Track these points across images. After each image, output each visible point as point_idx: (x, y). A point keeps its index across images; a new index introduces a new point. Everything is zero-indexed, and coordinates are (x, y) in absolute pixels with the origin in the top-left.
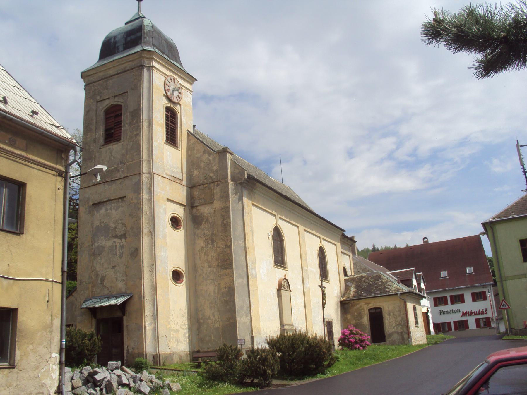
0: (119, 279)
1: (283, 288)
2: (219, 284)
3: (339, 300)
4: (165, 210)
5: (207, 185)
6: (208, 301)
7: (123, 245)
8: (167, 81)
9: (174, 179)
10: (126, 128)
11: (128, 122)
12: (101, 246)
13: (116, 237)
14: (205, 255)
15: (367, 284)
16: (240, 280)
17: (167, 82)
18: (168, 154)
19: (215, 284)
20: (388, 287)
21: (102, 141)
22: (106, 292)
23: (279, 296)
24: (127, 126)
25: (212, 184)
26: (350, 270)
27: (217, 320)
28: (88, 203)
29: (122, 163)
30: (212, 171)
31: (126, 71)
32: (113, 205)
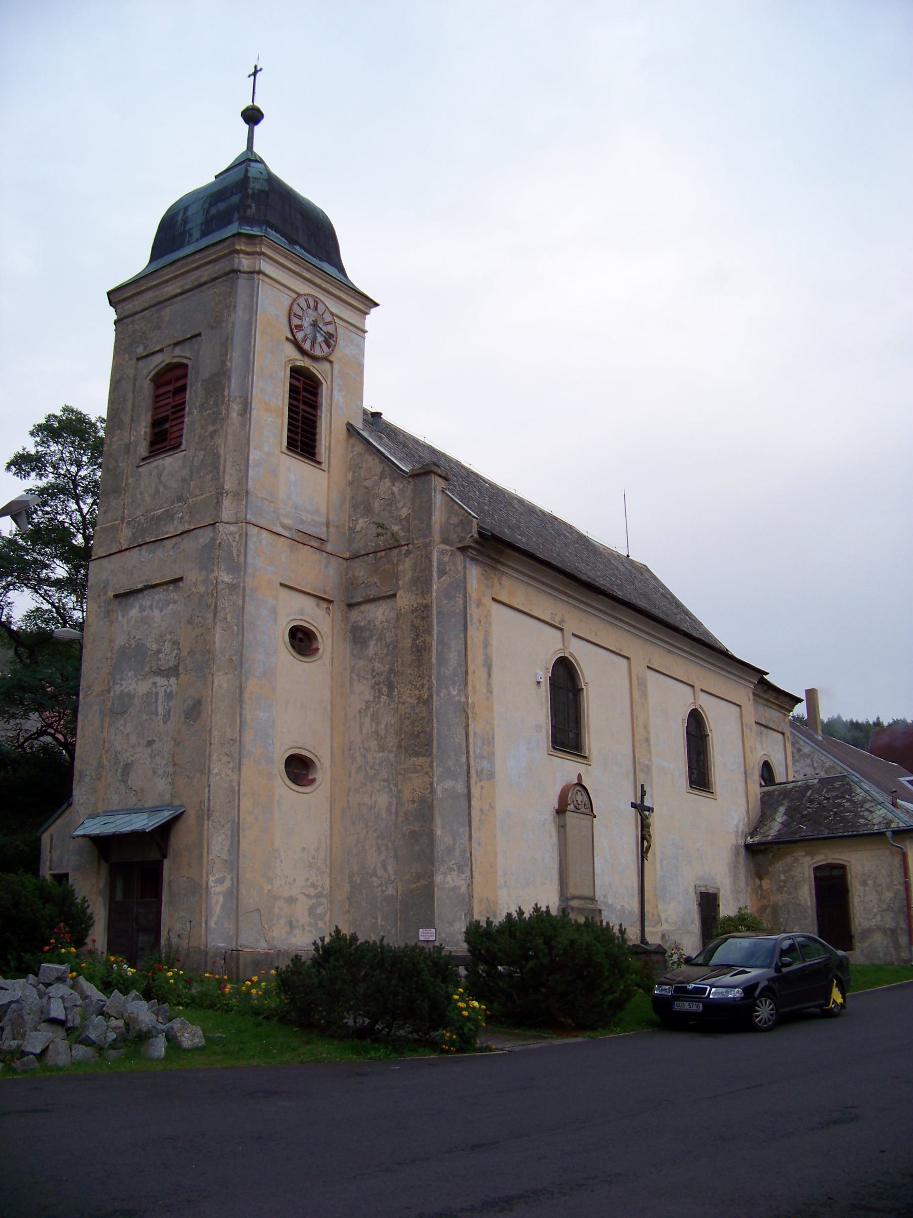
0: (160, 772)
1: (571, 807)
2: (400, 791)
3: (741, 842)
4: (274, 611)
5: (383, 553)
6: (375, 831)
7: (171, 692)
8: (295, 307)
9: (303, 539)
10: (193, 417)
11: (198, 404)
12: (128, 694)
13: (159, 672)
14: (372, 720)
15: (815, 805)
16: (448, 784)
17: (296, 309)
18: (292, 478)
19: (391, 791)
20: (866, 814)
21: (143, 449)
22: (132, 801)
23: (562, 828)
24: (195, 412)
25: (396, 551)
26: (783, 769)
27: (393, 878)
28: (105, 594)
29: (180, 499)
30: (398, 520)
31: (200, 285)
32: (157, 597)
